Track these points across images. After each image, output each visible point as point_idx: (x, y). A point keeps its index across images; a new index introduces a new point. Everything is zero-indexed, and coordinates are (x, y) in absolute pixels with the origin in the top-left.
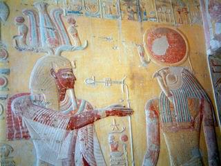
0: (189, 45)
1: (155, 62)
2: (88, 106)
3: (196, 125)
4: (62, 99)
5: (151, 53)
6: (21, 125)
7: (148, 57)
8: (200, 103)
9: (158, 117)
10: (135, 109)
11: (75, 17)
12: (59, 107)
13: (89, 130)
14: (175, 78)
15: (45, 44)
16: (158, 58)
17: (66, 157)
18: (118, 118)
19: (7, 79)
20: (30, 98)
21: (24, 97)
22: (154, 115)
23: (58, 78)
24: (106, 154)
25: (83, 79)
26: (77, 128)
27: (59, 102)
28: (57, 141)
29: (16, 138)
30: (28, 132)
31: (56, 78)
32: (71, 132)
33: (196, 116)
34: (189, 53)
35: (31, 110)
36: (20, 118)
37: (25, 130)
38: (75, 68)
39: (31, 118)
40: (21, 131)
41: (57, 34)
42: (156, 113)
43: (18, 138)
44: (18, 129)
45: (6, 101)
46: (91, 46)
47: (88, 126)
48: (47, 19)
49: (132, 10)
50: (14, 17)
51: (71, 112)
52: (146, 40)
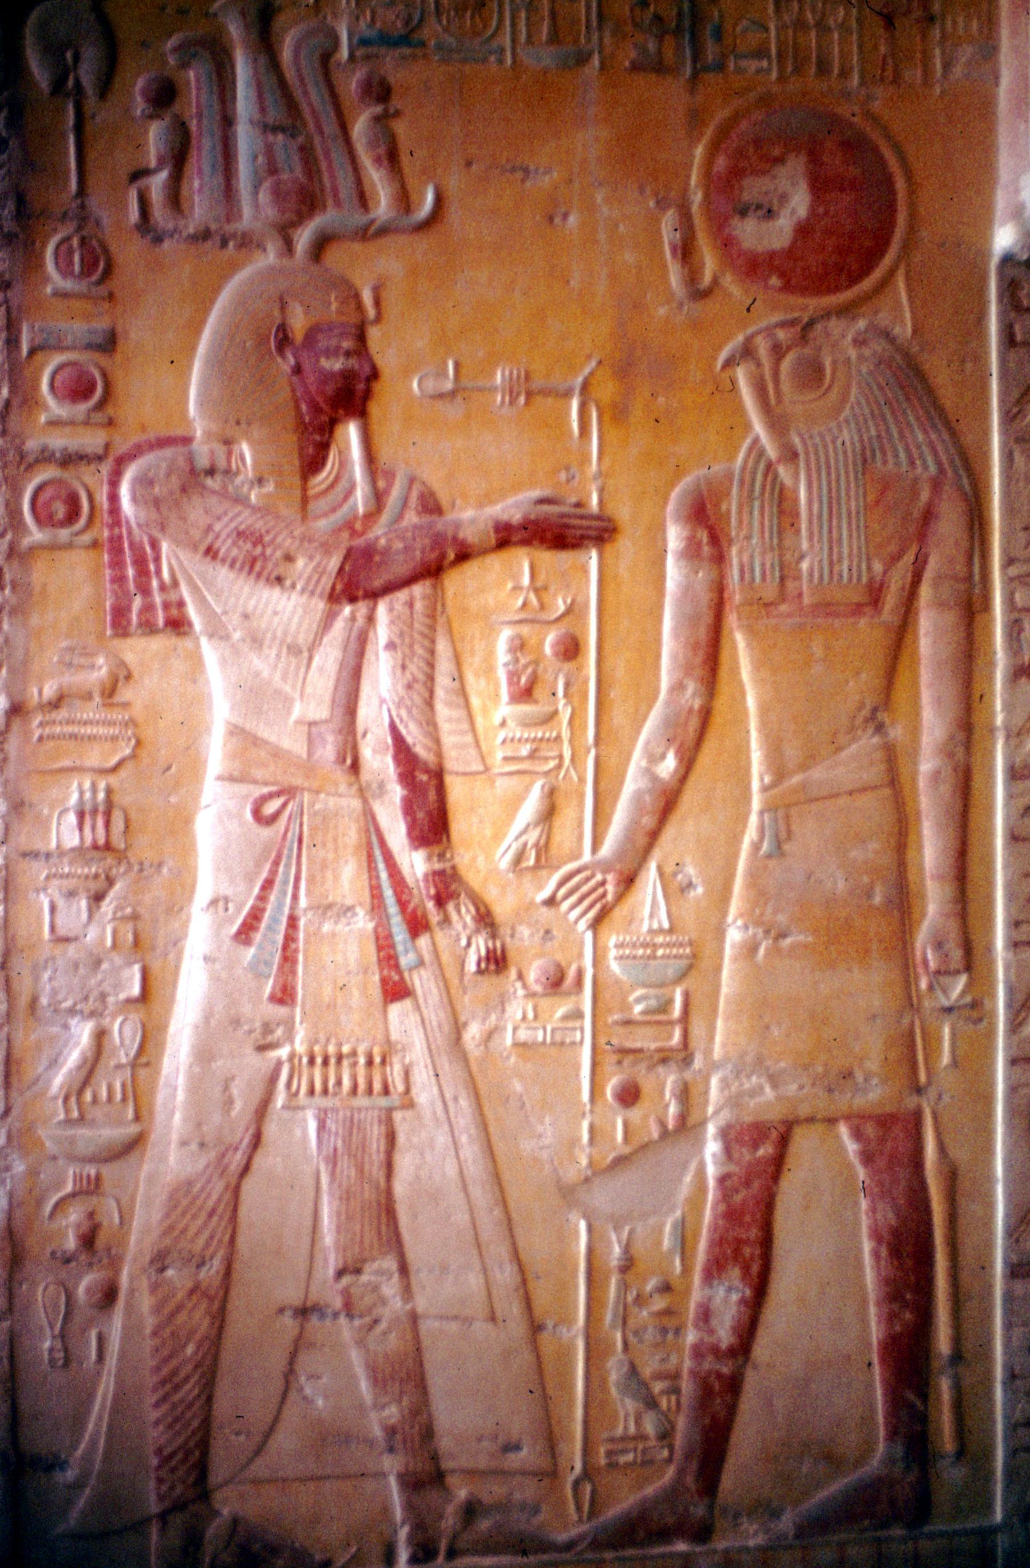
0: (912, 228)
2: (422, 497)
3: (891, 600)
4: (313, 464)
5: (727, 244)
6: (159, 571)
7: (709, 263)
8: (925, 495)
9: (720, 559)
10: (622, 512)
11: (394, 68)
12: (305, 500)
13: (419, 606)
15: (255, 207)
18: (549, 559)
19: (104, 375)
20: (190, 459)
21: (168, 452)
22: (706, 550)
23: (307, 366)
24: (485, 710)
25: (407, 373)
26: (374, 595)
28: (289, 648)
29: (140, 625)
30: (181, 604)
31: (298, 370)
32: (347, 610)
33: (895, 558)
34: (907, 247)
35: (196, 512)
36: (155, 545)
37: (173, 597)
38: (378, 319)
39: (195, 548)
40: (158, 599)
41: (306, 152)
42: (715, 540)
43: (148, 627)
44: (145, 590)
45: (106, 468)
46: (454, 214)
47: (419, 590)
48: (270, 81)
49: (658, 18)
50: (136, 88)
51: (349, 525)
52: (707, 173)
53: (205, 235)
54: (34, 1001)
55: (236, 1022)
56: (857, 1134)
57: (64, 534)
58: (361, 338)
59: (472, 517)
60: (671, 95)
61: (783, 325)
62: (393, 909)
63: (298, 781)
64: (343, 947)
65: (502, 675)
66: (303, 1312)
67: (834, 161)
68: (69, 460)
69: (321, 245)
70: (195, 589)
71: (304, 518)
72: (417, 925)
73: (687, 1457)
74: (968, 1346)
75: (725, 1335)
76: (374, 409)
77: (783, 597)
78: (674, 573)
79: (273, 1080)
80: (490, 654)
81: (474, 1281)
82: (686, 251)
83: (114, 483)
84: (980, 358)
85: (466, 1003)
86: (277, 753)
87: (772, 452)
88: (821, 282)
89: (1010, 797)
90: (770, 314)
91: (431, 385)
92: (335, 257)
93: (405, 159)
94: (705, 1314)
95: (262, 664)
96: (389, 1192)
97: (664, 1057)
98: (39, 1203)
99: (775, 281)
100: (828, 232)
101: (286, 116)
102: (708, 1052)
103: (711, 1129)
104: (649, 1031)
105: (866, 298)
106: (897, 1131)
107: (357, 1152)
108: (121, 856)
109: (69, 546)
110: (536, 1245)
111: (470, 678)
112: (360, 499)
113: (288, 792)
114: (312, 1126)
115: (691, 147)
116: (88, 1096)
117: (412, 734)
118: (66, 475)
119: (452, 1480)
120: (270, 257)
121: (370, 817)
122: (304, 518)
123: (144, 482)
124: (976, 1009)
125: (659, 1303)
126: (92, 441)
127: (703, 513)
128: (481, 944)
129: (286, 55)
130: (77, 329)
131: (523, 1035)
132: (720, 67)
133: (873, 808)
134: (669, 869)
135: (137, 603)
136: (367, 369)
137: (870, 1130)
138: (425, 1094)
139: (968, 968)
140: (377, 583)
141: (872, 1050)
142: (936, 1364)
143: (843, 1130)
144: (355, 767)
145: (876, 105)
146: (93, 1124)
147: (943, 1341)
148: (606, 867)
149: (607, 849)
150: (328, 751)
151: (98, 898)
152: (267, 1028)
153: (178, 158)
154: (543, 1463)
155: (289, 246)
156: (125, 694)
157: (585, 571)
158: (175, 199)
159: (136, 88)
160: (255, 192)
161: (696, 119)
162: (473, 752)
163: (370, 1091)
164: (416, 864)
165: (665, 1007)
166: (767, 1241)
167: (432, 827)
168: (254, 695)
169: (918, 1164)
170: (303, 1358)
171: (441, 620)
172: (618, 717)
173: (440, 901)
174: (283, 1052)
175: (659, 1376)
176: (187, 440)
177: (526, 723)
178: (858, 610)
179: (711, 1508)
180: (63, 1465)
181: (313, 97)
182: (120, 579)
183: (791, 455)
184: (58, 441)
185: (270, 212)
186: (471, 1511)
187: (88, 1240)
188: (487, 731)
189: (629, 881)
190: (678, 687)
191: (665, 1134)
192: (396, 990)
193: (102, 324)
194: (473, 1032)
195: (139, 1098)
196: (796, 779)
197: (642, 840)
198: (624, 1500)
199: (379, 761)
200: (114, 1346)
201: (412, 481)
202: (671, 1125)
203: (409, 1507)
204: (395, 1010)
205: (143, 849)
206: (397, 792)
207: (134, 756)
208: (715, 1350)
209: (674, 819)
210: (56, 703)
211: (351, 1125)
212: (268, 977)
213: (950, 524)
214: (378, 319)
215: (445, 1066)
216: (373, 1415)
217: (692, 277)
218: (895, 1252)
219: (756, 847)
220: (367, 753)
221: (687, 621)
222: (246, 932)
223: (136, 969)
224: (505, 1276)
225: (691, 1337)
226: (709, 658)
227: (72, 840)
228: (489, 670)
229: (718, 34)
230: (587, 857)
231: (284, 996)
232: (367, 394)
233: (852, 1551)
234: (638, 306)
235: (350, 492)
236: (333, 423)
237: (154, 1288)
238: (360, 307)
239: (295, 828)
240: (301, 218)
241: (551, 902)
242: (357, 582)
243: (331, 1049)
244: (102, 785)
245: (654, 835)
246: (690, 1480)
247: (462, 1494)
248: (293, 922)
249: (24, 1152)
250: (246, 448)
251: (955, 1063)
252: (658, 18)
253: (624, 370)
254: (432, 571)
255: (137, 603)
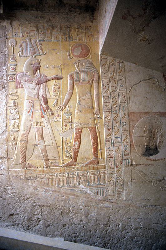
0: (91, 52)
1: (74, 58)
8: (93, 74)
9: (73, 80)
10: (64, 77)
11: (42, 42)
14: (83, 64)
16: (76, 56)
17: (36, 94)
18: (57, 81)
26: (41, 84)
27: (34, 75)
31: (33, 66)
34: (91, 54)
35: (24, 78)
36: (20, 81)
37: (22, 85)
40: (20, 85)
41: (34, 50)
42: (73, 78)
44: (20, 85)
46: (47, 53)
49: (66, 37)
50: (19, 45)
51: (38, 78)
53: (25, 56)
54: (9, 119)
55: (28, 120)
56: (89, 129)
57: (12, 81)
58: (39, 64)
59: (49, 77)
60: (68, 43)
61: (79, 61)
62: (42, 110)
63: (33, 99)
64: (38, 114)
65: (53, 90)
66: (35, 145)
67: (83, 47)
68: (12, 75)
69: (35, 57)
70: (24, 84)
71: (34, 78)
72: (45, 111)
73: (73, 158)
74: (102, 148)
75: (77, 147)
76: (40, 69)
77: (80, 82)
78: (69, 81)
79: (31, 125)
80: (52, 88)
81: (51, 142)
82: (69, 55)
83: (17, 76)
84: (99, 63)
85: (50, 118)
86: (31, 97)
87: (78, 71)
88: (82, 57)
89: (103, 99)
90: (77, 59)
91: (45, 67)
92: (36, 57)
93: (43, 49)
94: (74, 145)
95: (30, 90)
96: (43, 134)
97: (69, 122)
98: (10, 136)
99: (78, 57)
100: (83, 53)
101: (32, 47)
102: (74, 122)
103: (74, 129)
104: (68, 120)
105: (88, 58)
106: (93, 128)
107: (39, 131)
108: (17, 106)
109: (12, 81)
110: (57, 139)
111: (50, 91)
112: (39, 76)
113: (33, 100)
114: (35, 129)
115: (70, 47)
116: (14, 127)
117: (44, 95)
118: (12, 76)
119: (50, 160)
120: (31, 58)
121: (40, 102)
122: (34, 78)
123: (19, 76)
124: (101, 118)
125: (70, 144)
126: (15, 73)
127: (72, 77)
128: (51, 113)
129: (32, 42)
130: (13, 64)
131: (55, 121)
132: (72, 41)
133: (89, 100)
134: (69, 106)
135: (19, 86)
136: (40, 66)
137: (90, 128)
138: (46, 125)
139: (100, 114)
140: (41, 83)
141: (91, 121)
142: (99, 150)
143: (88, 128)
144: (39, 98)
145: (88, 43)
146: (15, 129)
147: (99, 148)
148: (63, 106)
149: (63, 105)
150: (36, 97)
151: (15, 110)
152: (31, 120)
153: (22, 51)
154: (59, 159)
155: (32, 57)
156: (17, 93)
157: (60, 81)
158: (22, 54)
159: (19, 45)
160: (29, 52)
161: (70, 45)
162: (126, 81)
163: (41, 126)
164: (45, 106)
165: (69, 118)
166: (80, 138)
167: (46, 103)
168: (30, 93)
169: (96, 131)
170: (35, 149)
171: (47, 86)
172: (64, 93)
173: (47, 109)
174: (32, 123)
175: (70, 151)
176: (23, 72)
177: (55, 94)
178: (87, 83)
179: (76, 163)
180: (12, 159)
181: (34, 45)
182: (17, 84)
183: (80, 71)
184: (11, 73)
185: (31, 54)
186: (51, 163)
187: (14, 139)
188: (51, 94)
189: (65, 107)
190: (69, 91)
191: (70, 129)
192: (43, 117)
193: (16, 64)
194: (51, 121)
195: (18, 127)
196: (82, 98)
197: (66, 103)
198: (67, 162)
199: (41, 98)
200: (17, 148)
201: (44, 75)
202: (70, 128)
203: (45, 162)
204: (43, 118)
205: (19, 106)
206: (43, 100)
207: (18, 98)
208: (76, 148)
209: (69, 102)
210: (11, 94)
211: (39, 129)
212: (100, 54)
213: (96, 76)
214: (41, 62)
215: (48, 123)
216: (42, 154)
217: (70, 57)
218: (93, 140)
219: (78, 104)
220: (40, 97)
221: (70, 85)
222: (28, 113)
223: (18, 116)
224: (54, 142)
225: (73, 147)
226: (73, 88)
227: (12, 105)
228: (51, 90)
229: (72, 38)
230: (61, 105)
231: (32, 118)
232: (40, 68)
233: (91, 167)
234: (65, 60)
235: (38, 76)
236: (37, 70)
237: (20, 143)
238: (39, 61)
239: (33, 104)
240: (33, 55)
241: (58, 109)
242: (39, 83)
243: (37, 122)
244: (15, 101)
245: (68, 103)
246: (73, 160)
247: (51, 162)
248: (33, 111)
249: (8, 131)
250: (28, 73)
251: (99, 122)
252: (66, 37)
253: (64, 65)
254: (46, 82)
255: (19, 86)
